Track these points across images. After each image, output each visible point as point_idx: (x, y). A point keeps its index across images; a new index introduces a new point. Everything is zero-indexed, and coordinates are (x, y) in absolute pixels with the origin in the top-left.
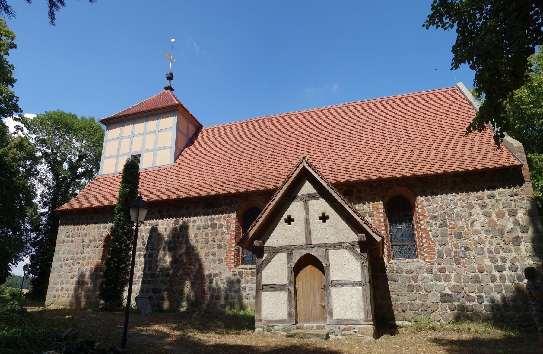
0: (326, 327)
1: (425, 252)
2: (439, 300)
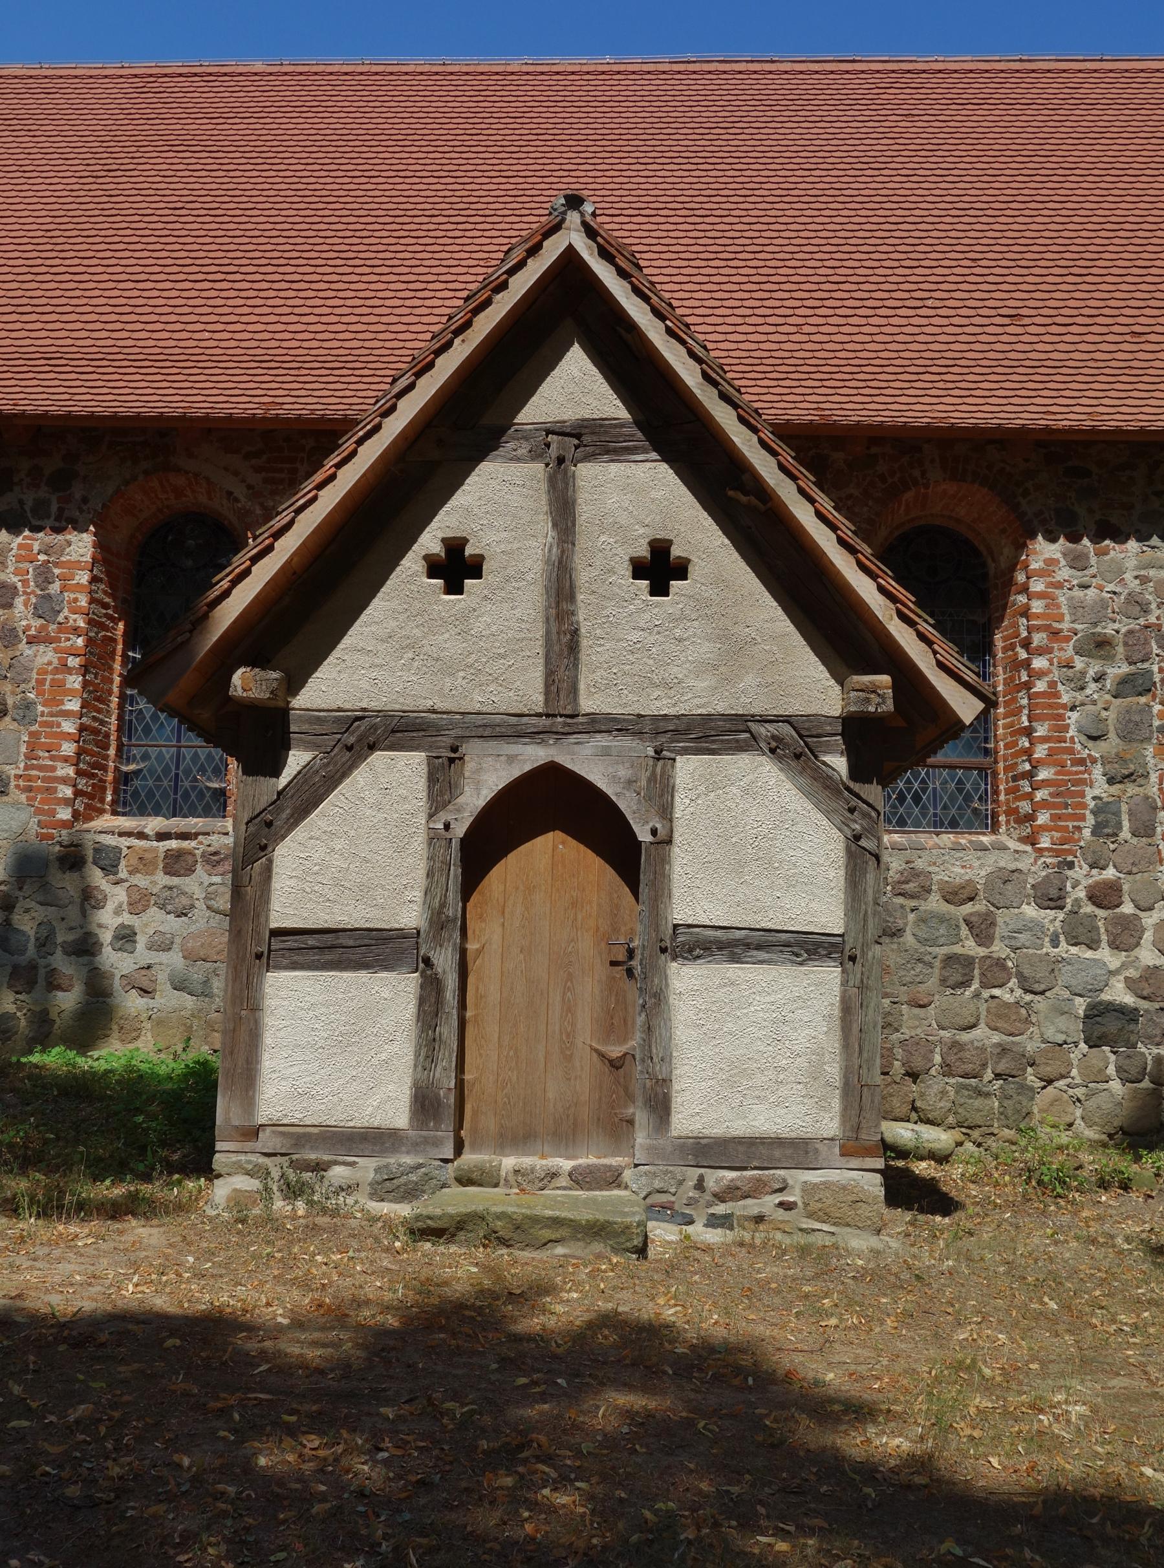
0: (628, 1175)
1: (1037, 807)
2: (1076, 1029)
